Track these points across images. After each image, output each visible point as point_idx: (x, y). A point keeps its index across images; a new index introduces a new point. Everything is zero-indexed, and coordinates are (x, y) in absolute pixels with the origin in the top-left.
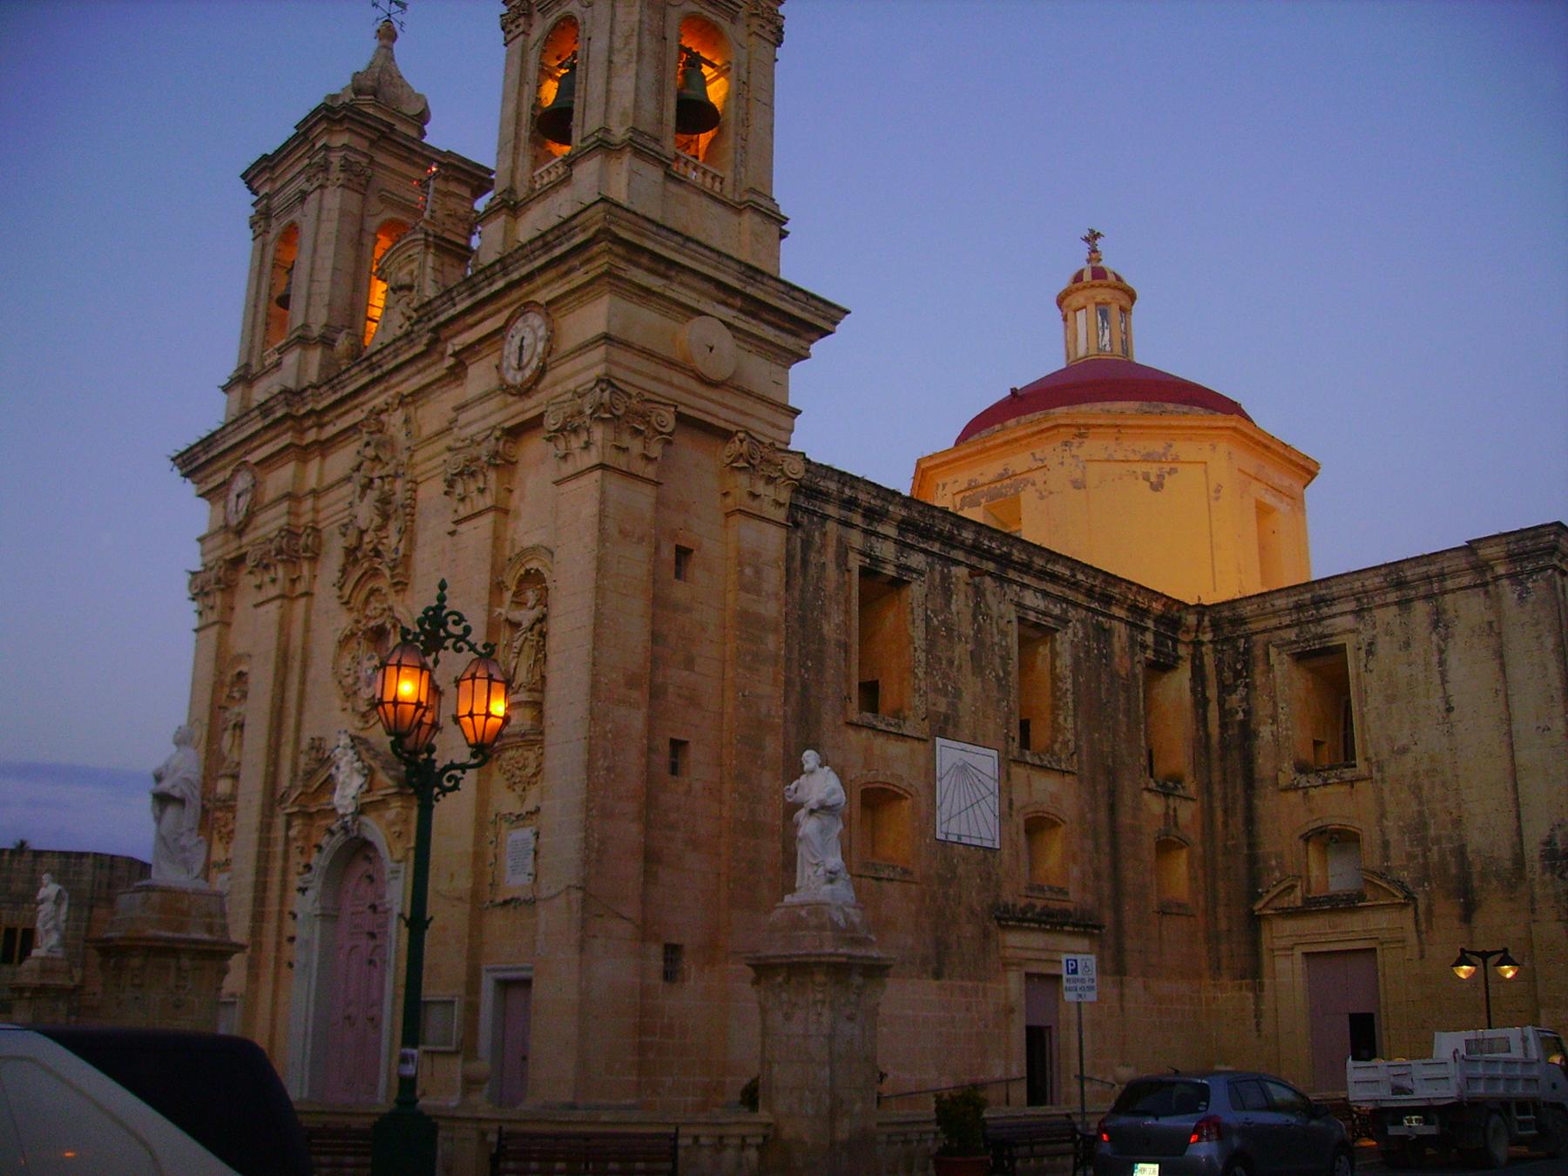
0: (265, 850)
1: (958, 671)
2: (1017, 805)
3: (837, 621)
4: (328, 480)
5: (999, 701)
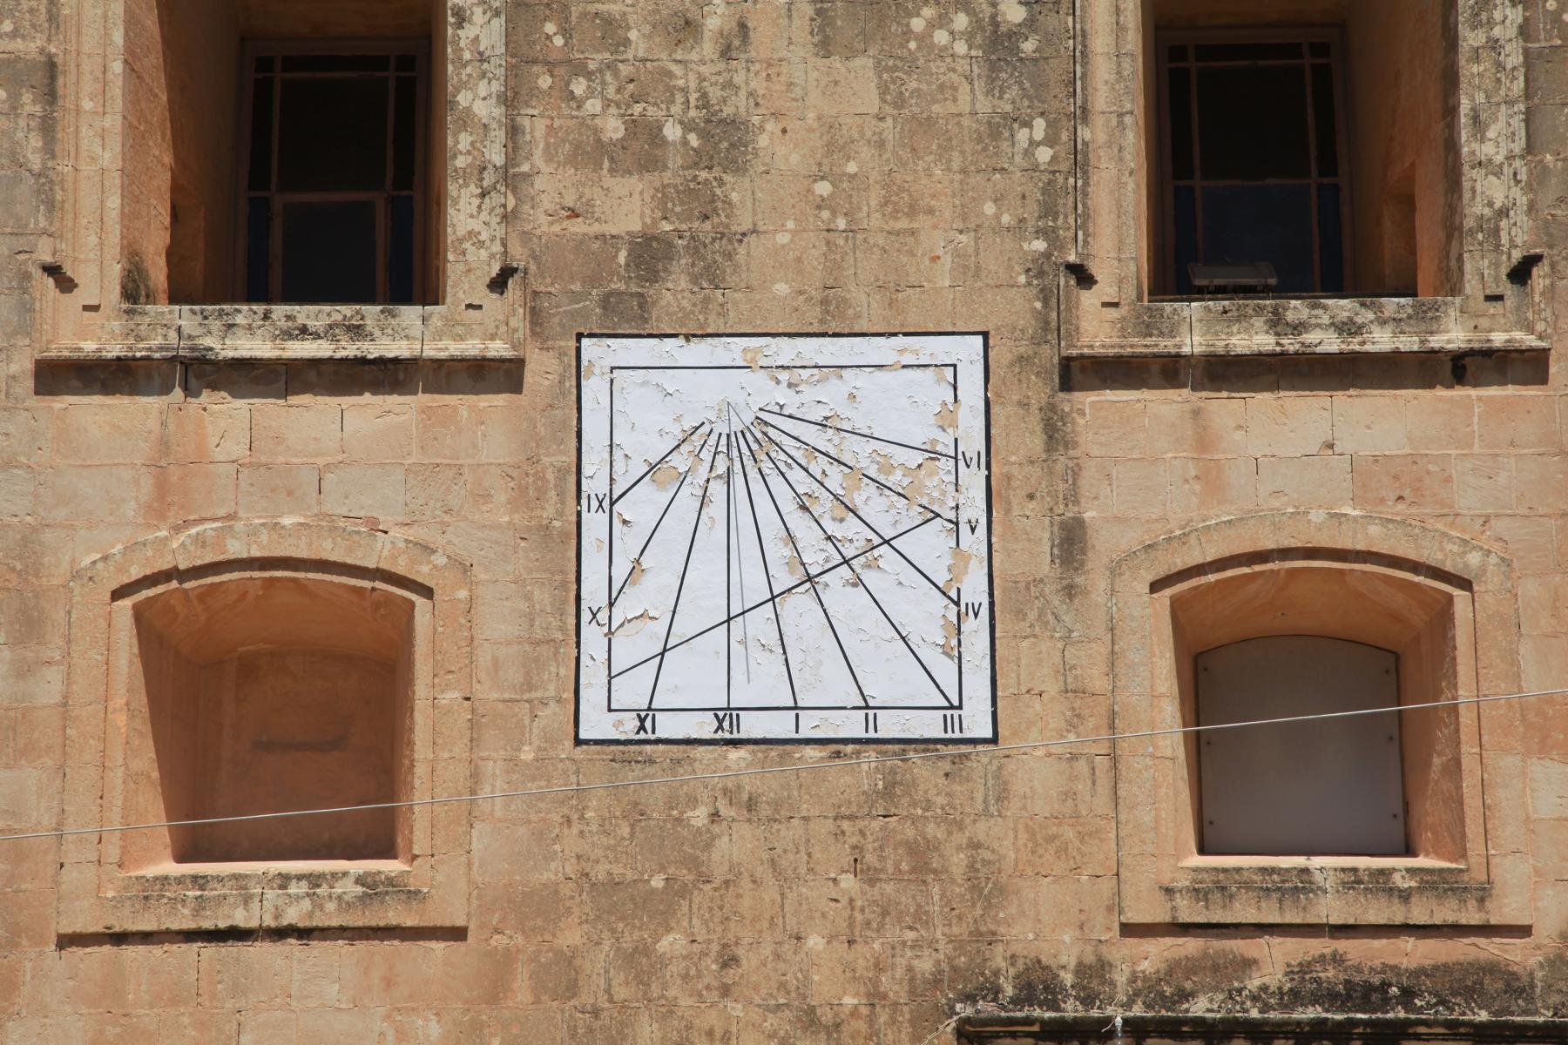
1: (726, 53)
2: (1106, 542)
5: (998, 128)
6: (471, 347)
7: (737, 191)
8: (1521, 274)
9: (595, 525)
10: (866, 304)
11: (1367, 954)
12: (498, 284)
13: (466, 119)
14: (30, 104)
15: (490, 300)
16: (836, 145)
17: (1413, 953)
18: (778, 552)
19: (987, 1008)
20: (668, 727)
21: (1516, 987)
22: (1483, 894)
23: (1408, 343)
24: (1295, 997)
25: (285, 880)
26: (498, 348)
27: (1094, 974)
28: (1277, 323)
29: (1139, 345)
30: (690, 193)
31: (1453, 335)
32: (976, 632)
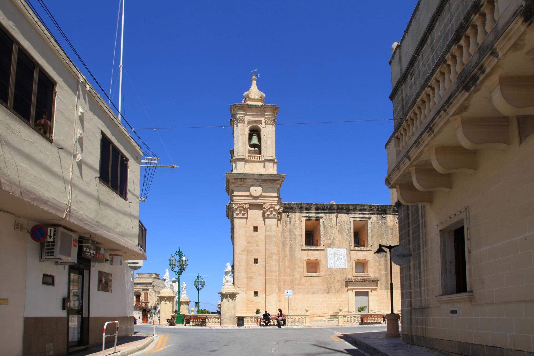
0: (403, 292)
1: (334, 234)
2: (352, 258)
3: (299, 231)
4: (501, 23)
5: (347, 238)
6: (322, 249)
7: (335, 241)
8: (371, 246)
9: (328, 257)
10: (341, 247)
11: (363, 277)
12: (323, 246)
13: (322, 237)
14: (301, 237)
15: (323, 246)
16: (339, 239)
17: (366, 277)
18: (337, 259)
19: (347, 280)
20: (332, 267)
21: (370, 279)
22: (369, 275)
23: (366, 249)
24: (360, 279)
25: (314, 274)
26: (324, 249)
27: (351, 278)
28: (360, 248)
29: (354, 249)
30: (332, 241)
31: (368, 249)
32: (346, 262)
